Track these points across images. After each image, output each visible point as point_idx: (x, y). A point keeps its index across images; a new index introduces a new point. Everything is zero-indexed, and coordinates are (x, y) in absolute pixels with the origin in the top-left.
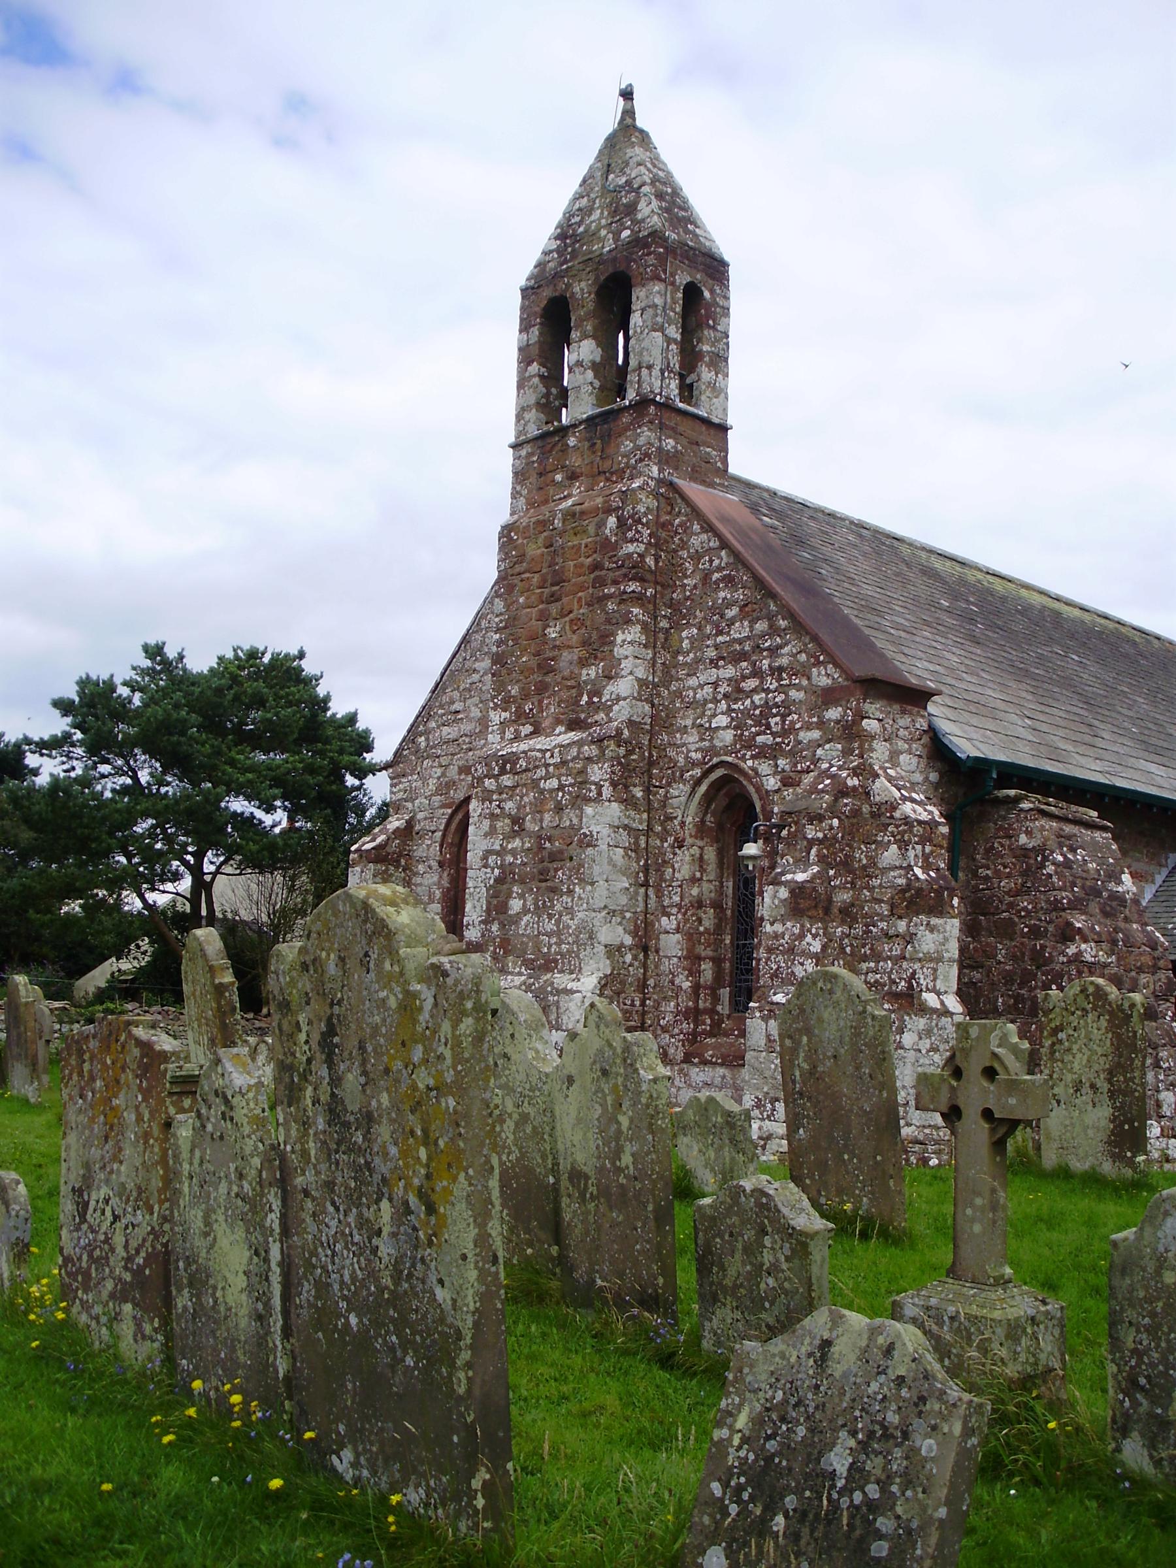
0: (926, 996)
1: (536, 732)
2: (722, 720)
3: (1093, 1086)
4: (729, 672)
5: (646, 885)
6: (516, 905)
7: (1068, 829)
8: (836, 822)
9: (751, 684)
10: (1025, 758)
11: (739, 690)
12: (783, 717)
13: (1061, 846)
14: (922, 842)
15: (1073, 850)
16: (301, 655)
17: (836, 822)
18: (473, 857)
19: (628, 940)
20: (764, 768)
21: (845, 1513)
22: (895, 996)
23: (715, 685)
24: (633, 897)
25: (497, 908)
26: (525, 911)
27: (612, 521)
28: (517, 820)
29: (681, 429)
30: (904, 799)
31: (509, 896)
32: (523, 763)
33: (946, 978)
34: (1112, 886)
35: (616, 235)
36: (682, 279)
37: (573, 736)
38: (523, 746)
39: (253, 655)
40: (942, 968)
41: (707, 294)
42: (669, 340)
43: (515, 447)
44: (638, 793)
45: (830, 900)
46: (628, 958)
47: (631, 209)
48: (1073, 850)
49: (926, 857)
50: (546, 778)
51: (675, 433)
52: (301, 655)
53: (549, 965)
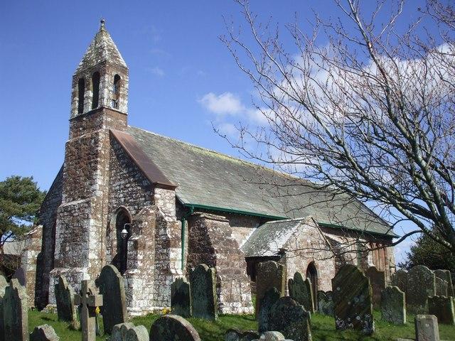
0: (171, 270)
1: (74, 200)
2: (122, 195)
3: (203, 294)
4: (123, 182)
5: (102, 242)
6: (67, 249)
7: (215, 222)
8: (146, 223)
9: (128, 185)
10: (205, 203)
11: (125, 187)
12: (136, 194)
13: (212, 227)
14: (170, 227)
15: (216, 228)
16: (32, 178)
17: (146, 223)
18: (57, 235)
19: (96, 257)
20: (131, 208)
21: (401, 291)
22: (164, 270)
23: (120, 185)
24: (98, 245)
25: (63, 250)
26: (70, 250)
27: (93, 141)
28: (68, 225)
29: (113, 115)
30: (166, 216)
31: (66, 246)
32: (69, 209)
33: (178, 265)
34: (227, 237)
35: (97, 61)
36: (114, 73)
37: (82, 201)
38: (70, 204)
39: (17, 178)
40: (176, 262)
41: (121, 78)
42: (110, 91)
43: (71, 120)
44: (99, 216)
45: (145, 245)
46: (97, 262)
47: (101, 54)
48: (216, 228)
49: (172, 232)
50: (75, 212)
51: (111, 116)
52: (32, 178)
53: (75, 265)
